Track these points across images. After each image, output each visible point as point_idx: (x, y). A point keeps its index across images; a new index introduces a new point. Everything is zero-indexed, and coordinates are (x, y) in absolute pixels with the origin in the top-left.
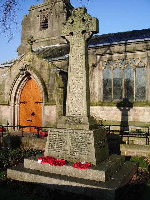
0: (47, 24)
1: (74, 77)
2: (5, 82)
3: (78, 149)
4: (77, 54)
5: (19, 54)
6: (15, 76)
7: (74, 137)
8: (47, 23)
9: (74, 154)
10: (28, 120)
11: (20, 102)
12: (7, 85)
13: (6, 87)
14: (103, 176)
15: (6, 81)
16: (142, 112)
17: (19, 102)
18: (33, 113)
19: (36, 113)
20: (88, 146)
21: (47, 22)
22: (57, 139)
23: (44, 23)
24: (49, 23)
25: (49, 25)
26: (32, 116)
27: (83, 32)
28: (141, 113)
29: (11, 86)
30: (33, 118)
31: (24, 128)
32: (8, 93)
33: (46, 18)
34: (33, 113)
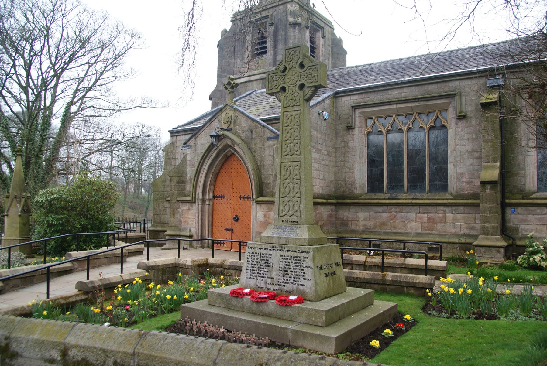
0: (266, 47)
1: (286, 160)
2: (186, 160)
3: (289, 276)
4: (292, 123)
5: (213, 105)
6: (204, 150)
7: (251, 255)
8: (264, 45)
9: (284, 284)
10: (227, 230)
11: (214, 197)
12: (190, 165)
13: (188, 170)
14: (322, 317)
15: (189, 158)
16: (441, 215)
17: (211, 197)
18: (236, 216)
19: (240, 218)
20: (304, 271)
21: (265, 42)
22: (259, 260)
23: (259, 44)
24: (268, 44)
25: (268, 49)
26: (234, 222)
27: (302, 86)
28: (439, 217)
29: (196, 168)
30: (236, 225)
31: (218, 243)
32: (191, 180)
33: (263, 34)
34: (236, 216)
